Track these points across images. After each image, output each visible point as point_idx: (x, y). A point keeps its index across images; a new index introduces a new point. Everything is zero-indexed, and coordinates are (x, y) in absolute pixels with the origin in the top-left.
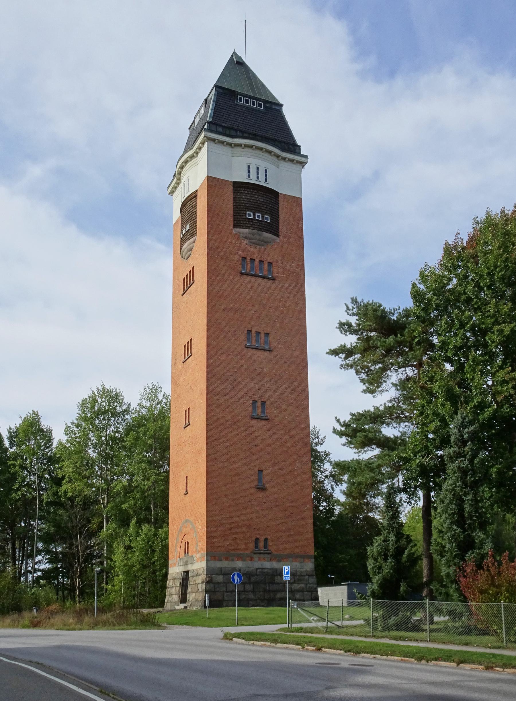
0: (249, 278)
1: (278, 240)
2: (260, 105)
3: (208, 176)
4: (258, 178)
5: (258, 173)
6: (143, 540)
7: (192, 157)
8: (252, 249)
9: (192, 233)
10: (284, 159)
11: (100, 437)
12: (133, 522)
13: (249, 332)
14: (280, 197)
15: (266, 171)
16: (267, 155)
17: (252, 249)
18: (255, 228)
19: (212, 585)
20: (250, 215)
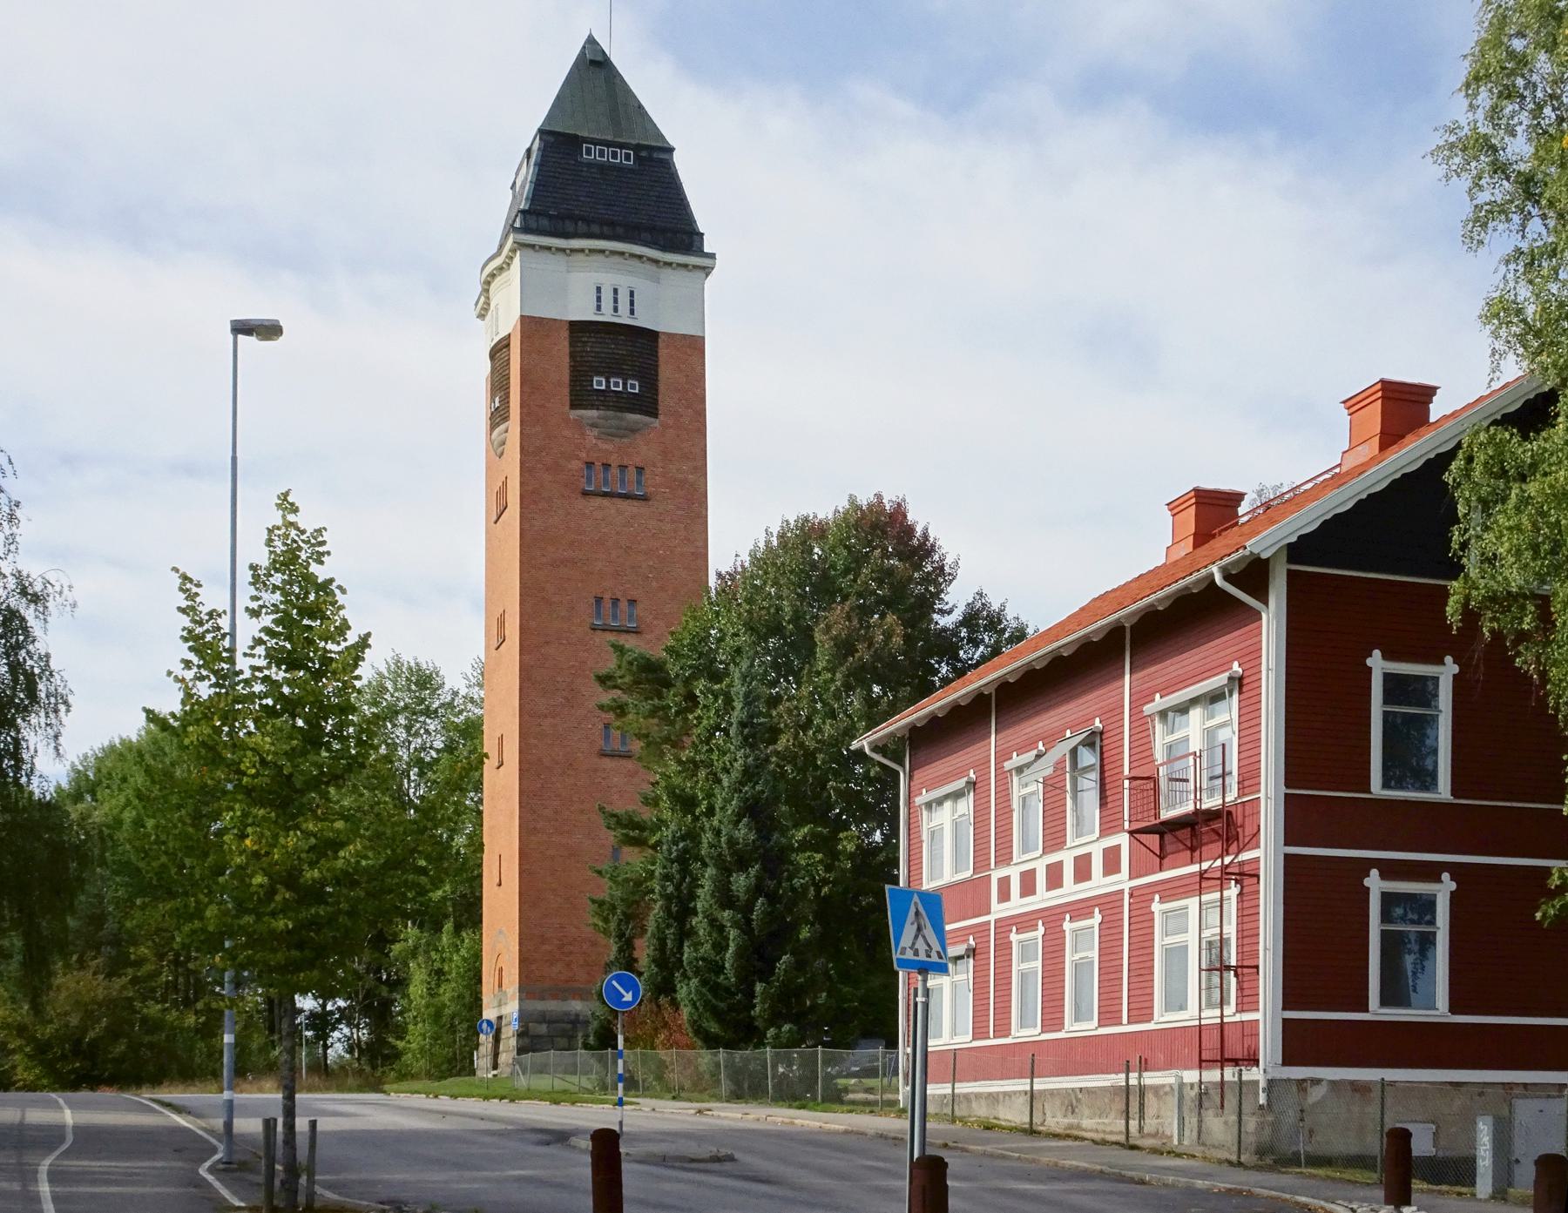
0: (598, 501)
1: (656, 423)
2: (628, 157)
3: (522, 317)
4: (616, 310)
5: (616, 300)
6: (464, 959)
7: (501, 269)
8: (605, 446)
10: (669, 264)
12: (448, 926)
13: (599, 600)
14: (662, 338)
15: (632, 294)
16: (636, 262)
17: (605, 446)
18: (608, 408)
19: (527, 1040)
20: (599, 383)
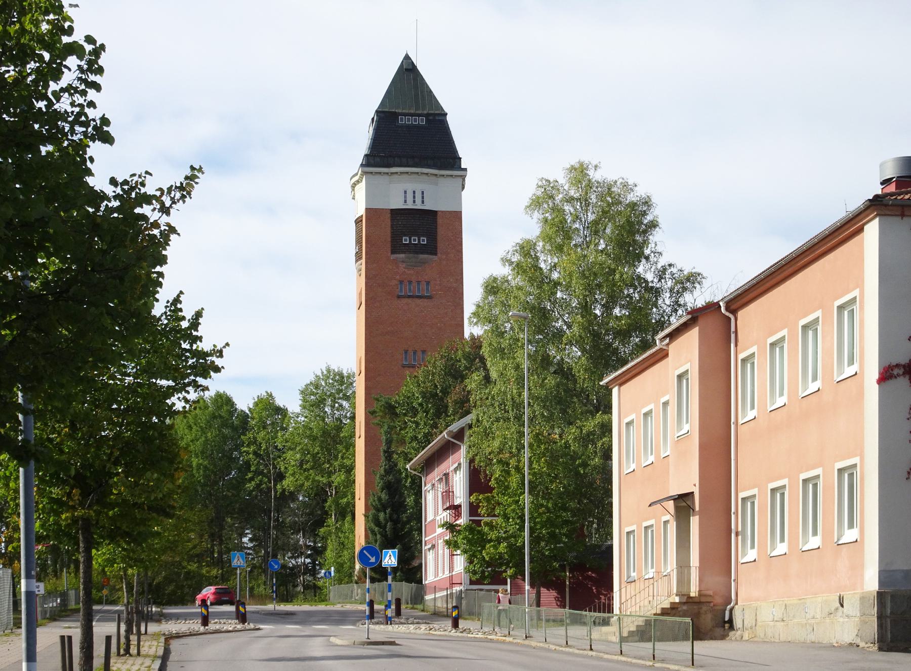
5: (414, 197)
9: (361, 258)
11: (318, 453)
15: (423, 193)
18: (410, 253)
